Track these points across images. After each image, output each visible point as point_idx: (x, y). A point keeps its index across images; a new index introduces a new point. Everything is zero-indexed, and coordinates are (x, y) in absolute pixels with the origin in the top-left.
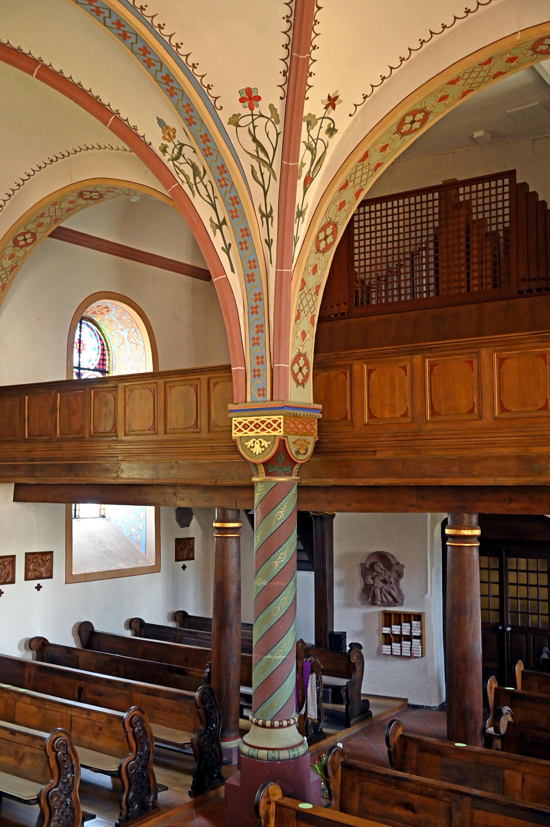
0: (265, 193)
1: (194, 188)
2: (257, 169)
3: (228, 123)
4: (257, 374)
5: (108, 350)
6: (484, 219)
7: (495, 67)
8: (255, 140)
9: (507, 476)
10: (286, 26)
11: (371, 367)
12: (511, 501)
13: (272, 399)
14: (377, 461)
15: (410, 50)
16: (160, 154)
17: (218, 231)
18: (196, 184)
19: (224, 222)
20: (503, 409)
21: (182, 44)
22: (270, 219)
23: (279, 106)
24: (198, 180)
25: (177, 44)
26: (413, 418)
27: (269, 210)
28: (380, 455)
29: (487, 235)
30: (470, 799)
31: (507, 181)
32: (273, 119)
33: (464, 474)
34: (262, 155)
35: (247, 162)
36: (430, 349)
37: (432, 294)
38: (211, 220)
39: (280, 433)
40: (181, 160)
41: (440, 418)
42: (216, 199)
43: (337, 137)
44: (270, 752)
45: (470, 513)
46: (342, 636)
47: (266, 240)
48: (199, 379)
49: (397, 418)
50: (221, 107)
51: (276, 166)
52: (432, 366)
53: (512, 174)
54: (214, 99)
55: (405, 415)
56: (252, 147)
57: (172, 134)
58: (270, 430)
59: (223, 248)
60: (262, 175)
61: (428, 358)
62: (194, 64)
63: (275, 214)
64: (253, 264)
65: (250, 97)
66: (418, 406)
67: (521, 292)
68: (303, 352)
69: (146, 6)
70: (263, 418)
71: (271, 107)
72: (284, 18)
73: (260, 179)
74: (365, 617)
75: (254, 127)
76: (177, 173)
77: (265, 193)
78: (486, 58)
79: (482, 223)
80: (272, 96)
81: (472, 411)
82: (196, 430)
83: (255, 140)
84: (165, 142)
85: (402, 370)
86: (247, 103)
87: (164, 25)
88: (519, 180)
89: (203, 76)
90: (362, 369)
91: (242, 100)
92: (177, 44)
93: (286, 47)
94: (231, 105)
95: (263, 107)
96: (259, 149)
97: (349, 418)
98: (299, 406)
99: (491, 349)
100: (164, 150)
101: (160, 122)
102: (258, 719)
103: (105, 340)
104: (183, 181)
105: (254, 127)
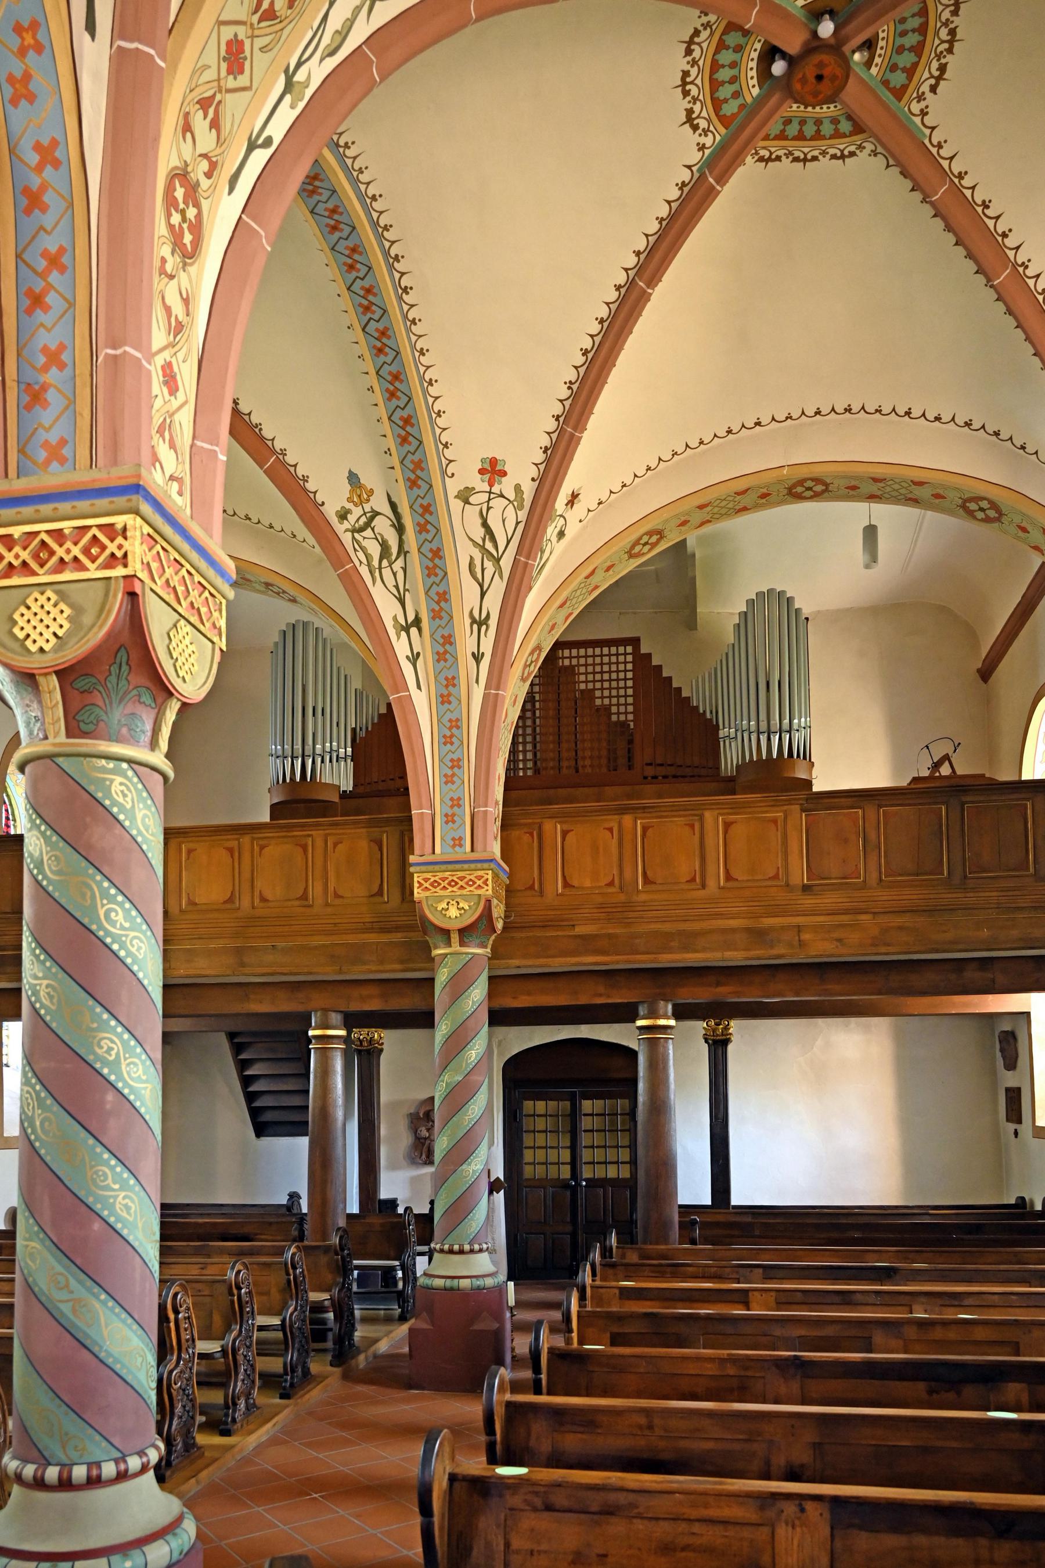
0: (483, 594)
1: (377, 574)
2: (478, 562)
3: (456, 497)
4: (449, 819)
5: (14, 820)
6: (594, 689)
7: (745, 500)
8: (485, 524)
9: (736, 950)
10: (565, 393)
11: (566, 827)
12: (718, 984)
13: (472, 850)
14: (576, 936)
15: (660, 459)
16: (334, 520)
17: (403, 634)
18: (380, 568)
19: (417, 622)
20: (729, 877)
22: (484, 628)
23: (529, 490)
24: (385, 563)
25: (431, 380)
26: (621, 888)
27: (483, 616)
28: (579, 930)
29: (598, 710)
30: (761, 1270)
31: (629, 649)
32: (515, 503)
33: (685, 948)
34: (489, 546)
35: (466, 551)
36: (644, 808)
37: (529, 773)
38: (395, 618)
39: (488, 891)
40: (368, 533)
41: (653, 887)
43: (564, 541)
44: (474, 1280)
45: (667, 1001)
46: (393, 1203)
47: (473, 654)
49: (600, 887)
50: (453, 475)
51: (506, 563)
52: (645, 829)
53: (635, 642)
55: (611, 884)
56: (478, 533)
57: (365, 496)
58: (472, 889)
59: (407, 657)
60: (483, 570)
61: (640, 818)
62: (439, 411)
63: (493, 622)
64: (452, 682)
65: (493, 470)
66: (628, 874)
67: (645, 778)
70: (460, 874)
71: (518, 488)
73: (479, 576)
74: (414, 1181)
75: (489, 509)
76: (355, 550)
77: (483, 594)
78: (744, 487)
79: (589, 694)
80: (522, 474)
81: (693, 880)
82: (306, 903)
83: (485, 524)
84: (349, 506)
85: (608, 833)
86: (487, 477)
87: (428, 350)
88: (644, 650)
89: (444, 429)
90: (553, 829)
91: (482, 472)
92: (431, 380)
93: (557, 418)
94: (466, 473)
95: (506, 486)
97: (536, 887)
99: (718, 811)
100: (343, 516)
101: (353, 478)
102: (443, 1245)
103: (11, 805)
104: (361, 562)
105: (489, 509)
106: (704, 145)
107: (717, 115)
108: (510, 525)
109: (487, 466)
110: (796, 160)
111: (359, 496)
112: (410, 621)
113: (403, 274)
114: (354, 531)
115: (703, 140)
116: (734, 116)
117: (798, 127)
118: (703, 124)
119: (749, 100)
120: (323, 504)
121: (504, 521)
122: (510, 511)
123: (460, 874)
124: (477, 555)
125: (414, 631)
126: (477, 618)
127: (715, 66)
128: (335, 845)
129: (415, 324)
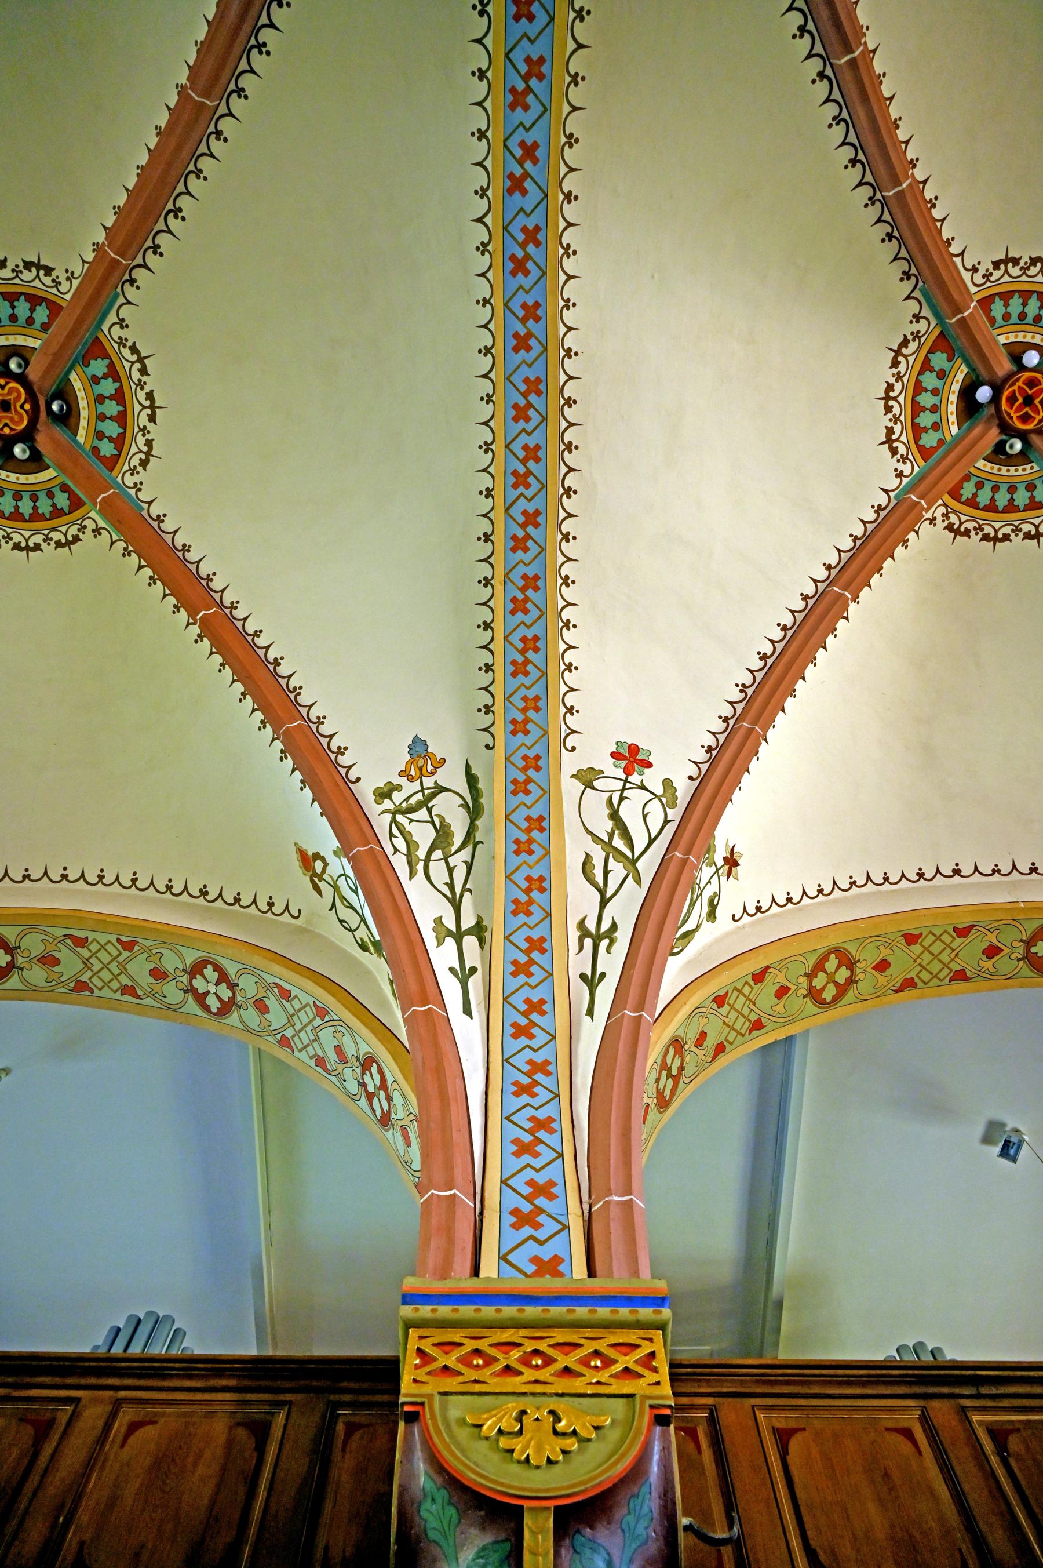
0: (604, 903)
1: (420, 867)
8: (614, 816)
13: (591, 1273)
17: (450, 942)
18: (427, 861)
21: (575, 626)
22: (605, 943)
23: (684, 789)
25: (568, 621)
27: (605, 926)
32: (664, 800)
34: (618, 843)
38: (439, 921)
40: (422, 814)
42: (467, 894)
48: (78, 1400)
50: (574, 749)
51: (647, 866)
54: (568, 731)
56: (603, 826)
57: (430, 768)
60: (606, 873)
62: (571, 664)
68: (1021, 949)
69: (574, 538)
70: (561, 1336)
71: (667, 783)
72: (737, 685)
73: (599, 879)
75: (622, 799)
77: (604, 903)
80: (676, 764)
83: (614, 816)
86: (623, 763)
95: (653, 778)
96: (617, 832)
98: (793, 1363)
101: (418, 748)
105: (622, 799)
106: (902, 472)
107: (916, 443)
108: (655, 823)
109: (624, 751)
110: (986, 538)
111: (421, 769)
112: (463, 928)
113: (571, 470)
114: (398, 811)
115: (900, 466)
116: (934, 450)
117: (990, 494)
118: (902, 450)
119: (948, 438)
120: (358, 779)
121: (645, 817)
122: (656, 811)
123: (561, 1336)
124: (598, 855)
125: (470, 942)
126: (592, 928)
127: (919, 388)
128: (134, 1427)
129: (568, 541)
